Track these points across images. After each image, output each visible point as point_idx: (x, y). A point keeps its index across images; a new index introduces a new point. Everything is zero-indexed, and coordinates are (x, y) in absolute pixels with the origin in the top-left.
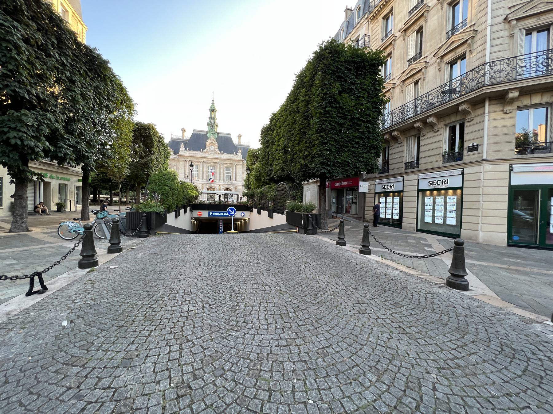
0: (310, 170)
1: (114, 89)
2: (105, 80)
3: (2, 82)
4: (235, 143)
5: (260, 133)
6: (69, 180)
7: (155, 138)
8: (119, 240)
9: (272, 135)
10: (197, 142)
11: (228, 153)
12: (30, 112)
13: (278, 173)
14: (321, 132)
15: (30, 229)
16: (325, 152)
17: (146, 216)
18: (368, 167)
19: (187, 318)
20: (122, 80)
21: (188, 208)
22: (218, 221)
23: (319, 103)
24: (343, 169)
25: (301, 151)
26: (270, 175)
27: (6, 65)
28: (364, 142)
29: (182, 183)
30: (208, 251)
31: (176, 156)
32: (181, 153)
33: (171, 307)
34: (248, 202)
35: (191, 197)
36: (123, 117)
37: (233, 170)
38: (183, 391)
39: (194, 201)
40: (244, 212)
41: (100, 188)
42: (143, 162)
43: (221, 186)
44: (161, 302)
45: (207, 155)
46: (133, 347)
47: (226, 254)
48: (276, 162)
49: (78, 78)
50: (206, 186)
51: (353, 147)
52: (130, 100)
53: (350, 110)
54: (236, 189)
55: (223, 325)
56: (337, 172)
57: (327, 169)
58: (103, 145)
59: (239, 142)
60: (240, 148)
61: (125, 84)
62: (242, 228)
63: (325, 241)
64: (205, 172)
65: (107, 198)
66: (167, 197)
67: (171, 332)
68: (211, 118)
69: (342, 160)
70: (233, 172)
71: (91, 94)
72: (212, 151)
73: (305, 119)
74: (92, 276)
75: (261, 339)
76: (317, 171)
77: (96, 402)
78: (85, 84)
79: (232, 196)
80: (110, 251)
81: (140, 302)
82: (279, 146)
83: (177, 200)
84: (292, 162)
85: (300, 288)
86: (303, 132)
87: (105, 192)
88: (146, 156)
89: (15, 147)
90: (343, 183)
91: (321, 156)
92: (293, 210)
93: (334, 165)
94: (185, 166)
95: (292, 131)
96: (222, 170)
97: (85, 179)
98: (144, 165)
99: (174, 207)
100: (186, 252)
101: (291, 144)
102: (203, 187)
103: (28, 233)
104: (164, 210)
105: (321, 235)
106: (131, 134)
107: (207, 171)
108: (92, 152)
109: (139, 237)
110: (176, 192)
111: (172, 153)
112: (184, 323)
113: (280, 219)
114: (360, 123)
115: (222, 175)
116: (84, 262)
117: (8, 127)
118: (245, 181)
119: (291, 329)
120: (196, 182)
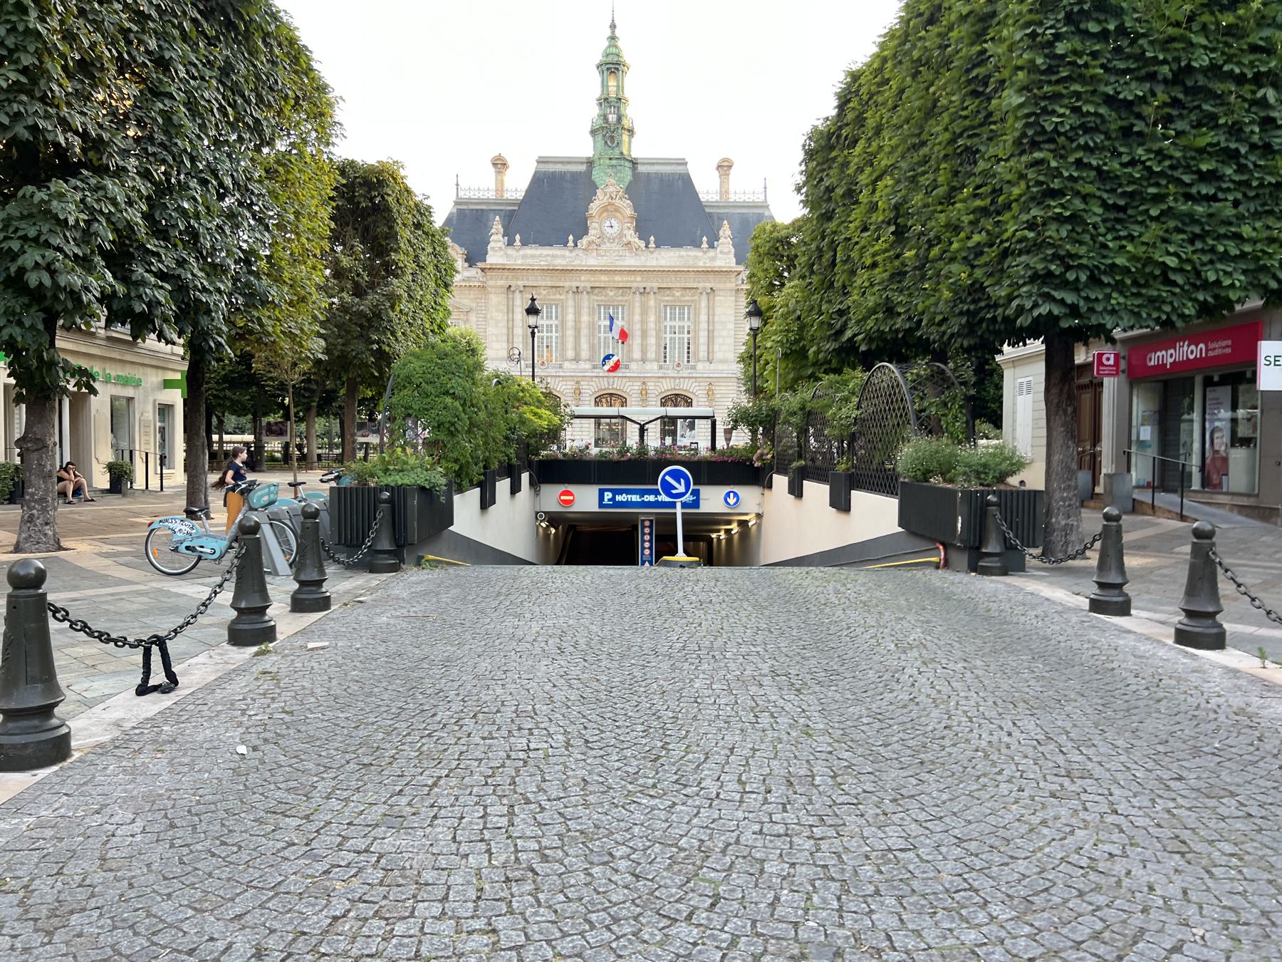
0: (996, 306)
1: (274, 63)
2: (248, 36)
3: (8, 109)
4: (703, 197)
5: (801, 155)
6: (137, 384)
7: (403, 217)
8: (322, 572)
9: (846, 164)
10: (554, 205)
11: (676, 244)
12: (66, 182)
13: (870, 323)
14: (1035, 145)
15: (64, 544)
16: (1051, 231)
17: (390, 501)
18: (1264, 279)
19: (525, 762)
20: (295, 23)
21: (525, 477)
22: (636, 527)
23: (1028, 25)
24: (1138, 295)
25: (956, 229)
26: (841, 332)
27: (16, 56)
28: (1241, 169)
29: (502, 381)
30: (591, 611)
31: (473, 272)
32: (493, 258)
33: (484, 739)
34: (754, 447)
35: (534, 434)
36: (301, 155)
37: (697, 314)
38: (518, 874)
39: (545, 447)
40: (737, 489)
41: (224, 409)
42: (364, 306)
43: (651, 385)
44: (457, 728)
45: (592, 261)
46: (404, 801)
47: (649, 624)
48: (862, 278)
49: (178, 50)
50: (590, 390)
51: (1188, 197)
52: (322, 89)
53: (1172, 39)
54: (710, 394)
55: (617, 783)
56: (1113, 312)
57: (1062, 302)
58: (248, 258)
59: (724, 191)
60: (727, 217)
61: (306, 37)
62: (710, 544)
63: (1049, 596)
64: (584, 332)
65: (247, 444)
66: (452, 434)
67: (486, 783)
68: (605, 101)
69: (1133, 258)
70: (697, 322)
71: (211, 94)
72: (612, 240)
73: (975, 94)
74: (268, 663)
75: (716, 816)
76: (1021, 310)
77: (347, 866)
78: (195, 65)
79: (692, 427)
80: (299, 605)
81: (404, 725)
82: (873, 207)
83: (486, 443)
84: (923, 278)
85: (877, 725)
86: (967, 149)
87: (231, 420)
88: (372, 286)
89: (37, 295)
90: (1188, 351)
91: (1033, 248)
92: (927, 474)
93: (1094, 280)
94: (510, 310)
95: (923, 144)
96: (652, 318)
97: (194, 380)
98: (369, 320)
99: (476, 470)
100: (519, 616)
101: (917, 199)
102: (578, 393)
103: (61, 554)
104: (443, 481)
105: (1040, 578)
106: (325, 213)
107: (593, 327)
108: (219, 291)
109: (371, 572)
110: (482, 415)
111: (460, 264)
112: (517, 770)
113: (876, 514)
114: (1219, 87)
115: (652, 340)
116: (241, 627)
117: (20, 238)
118: (742, 359)
119: (809, 808)
120: (552, 372)
